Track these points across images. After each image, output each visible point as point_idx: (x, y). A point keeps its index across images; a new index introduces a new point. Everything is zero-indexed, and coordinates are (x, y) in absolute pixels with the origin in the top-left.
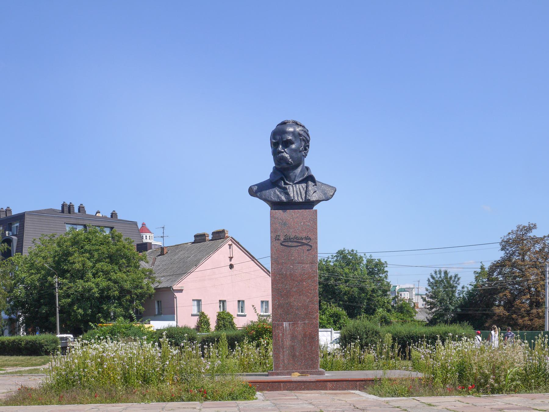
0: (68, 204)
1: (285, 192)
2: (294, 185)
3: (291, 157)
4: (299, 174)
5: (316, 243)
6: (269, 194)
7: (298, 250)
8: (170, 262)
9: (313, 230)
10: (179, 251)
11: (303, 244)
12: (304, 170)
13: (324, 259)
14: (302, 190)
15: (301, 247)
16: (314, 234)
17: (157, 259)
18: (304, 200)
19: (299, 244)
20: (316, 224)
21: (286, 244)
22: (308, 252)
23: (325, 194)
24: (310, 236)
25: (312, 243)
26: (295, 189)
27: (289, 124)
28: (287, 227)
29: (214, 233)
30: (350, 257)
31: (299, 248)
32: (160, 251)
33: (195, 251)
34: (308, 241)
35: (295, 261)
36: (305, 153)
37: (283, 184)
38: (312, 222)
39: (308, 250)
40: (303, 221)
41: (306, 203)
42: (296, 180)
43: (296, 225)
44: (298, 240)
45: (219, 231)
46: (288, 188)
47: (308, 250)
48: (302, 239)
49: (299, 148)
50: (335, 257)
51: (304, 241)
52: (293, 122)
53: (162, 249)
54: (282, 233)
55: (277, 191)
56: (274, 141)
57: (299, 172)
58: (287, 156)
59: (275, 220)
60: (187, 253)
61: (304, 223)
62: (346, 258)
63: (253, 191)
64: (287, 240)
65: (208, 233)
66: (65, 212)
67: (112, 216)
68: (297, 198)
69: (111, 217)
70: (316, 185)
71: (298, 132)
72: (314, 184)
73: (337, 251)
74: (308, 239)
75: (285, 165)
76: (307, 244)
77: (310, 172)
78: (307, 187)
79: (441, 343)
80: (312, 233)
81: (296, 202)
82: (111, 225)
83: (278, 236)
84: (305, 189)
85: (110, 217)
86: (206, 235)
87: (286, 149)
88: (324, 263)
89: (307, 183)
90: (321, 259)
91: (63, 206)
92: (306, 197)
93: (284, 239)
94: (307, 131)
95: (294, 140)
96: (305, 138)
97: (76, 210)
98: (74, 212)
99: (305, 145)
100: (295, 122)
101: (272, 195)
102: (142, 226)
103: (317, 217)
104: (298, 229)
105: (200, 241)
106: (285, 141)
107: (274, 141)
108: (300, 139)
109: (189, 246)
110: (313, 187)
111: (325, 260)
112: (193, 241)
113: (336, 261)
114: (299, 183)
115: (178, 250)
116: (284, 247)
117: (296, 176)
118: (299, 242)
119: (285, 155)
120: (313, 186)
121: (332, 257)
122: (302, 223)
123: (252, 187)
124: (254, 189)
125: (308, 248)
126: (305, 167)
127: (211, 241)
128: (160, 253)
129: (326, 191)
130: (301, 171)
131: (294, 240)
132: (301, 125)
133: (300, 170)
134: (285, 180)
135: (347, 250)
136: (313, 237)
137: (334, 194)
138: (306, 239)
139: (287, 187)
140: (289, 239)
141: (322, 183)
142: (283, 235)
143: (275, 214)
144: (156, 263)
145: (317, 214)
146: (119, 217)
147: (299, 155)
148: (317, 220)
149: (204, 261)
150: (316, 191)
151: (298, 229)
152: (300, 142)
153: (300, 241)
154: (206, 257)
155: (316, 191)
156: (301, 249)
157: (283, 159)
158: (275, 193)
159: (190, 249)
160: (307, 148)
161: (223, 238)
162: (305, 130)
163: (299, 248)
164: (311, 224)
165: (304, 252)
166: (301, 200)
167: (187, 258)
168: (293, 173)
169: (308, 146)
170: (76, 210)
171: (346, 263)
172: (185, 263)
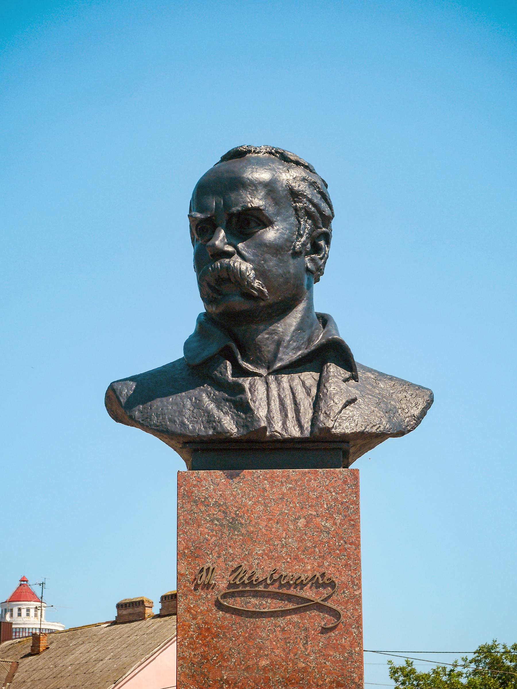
1: (234, 402)
2: (271, 378)
3: (260, 273)
4: (292, 336)
5: (358, 601)
6: (175, 408)
7: (283, 629)
8: (50, 673)
9: (346, 550)
10: (77, 645)
12: (311, 326)
13: (444, 669)
14: (301, 394)
15: (295, 618)
16: (346, 565)
17: (20, 666)
18: (307, 433)
19: (291, 606)
20: (355, 526)
21: (237, 603)
22: (323, 639)
23: (391, 412)
24: (331, 572)
25: (338, 602)
26: (274, 392)
27: (258, 158)
28: (242, 535)
29: (164, 599)
30: (509, 664)
31: (289, 623)
32: (30, 643)
33: (116, 643)
34: (326, 592)
35: (270, 675)
36: (312, 260)
37: (229, 372)
38: (338, 518)
39: (325, 630)
40: (304, 512)
41: (314, 442)
42: (281, 360)
43: (278, 530)
44: (284, 591)
46: (247, 386)
47: (325, 630)
48: (302, 585)
49: (289, 241)
50: (471, 663)
51: (308, 593)
52: (270, 153)
53: (36, 638)
54: (222, 559)
55: (207, 399)
56: (199, 215)
57: (293, 328)
58: (243, 268)
59: (195, 510)
60: (96, 649)
61: (309, 520)
62: (501, 664)
63: (120, 401)
64: (240, 589)
65: (151, 599)
68: (280, 424)
70: (355, 378)
71: (288, 185)
72: (348, 374)
73: (476, 648)
74: (324, 585)
76: (320, 607)
77: (334, 332)
78: (320, 384)
80: (341, 563)
81: (278, 441)
83: (204, 573)
84: (314, 391)
86: (146, 604)
87: (240, 245)
88: (444, 678)
89: (320, 371)
90: (438, 668)
92: (314, 420)
93: (230, 586)
94: (320, 183)
95: (270, 210)
96: (315, 205)
99: (315, 233)
100: (277, 152)
101: (188, 413)
102: (21, 585)
103: (358, 496)
104: (283, 546)
105: (131, 618)
106: (239, 214)
107: (199, 215)
108: (296, 209)
109: (102, 632)
110: (343, 385)
111: (448, 670)
112: (114, 619)
113: (475, 672)
115: (74, 643)
116: (228, 615)
117: (279, 344)
118: (290, 598)
119: (237, 262)
120: (346, 380)
121: (463, 663)
122: (302, 520)
123: (116, 386)
124: (121, 393)
125: (327, 620)
126: (315, 315)
127: (159, 619)
128: (28, 650)
129: (393, 400)
130: (300, 328)
131: (271, 589)
132: (298, 163)
133: (294, 324)
134: (239, 356)
135: (501, 647)
136: (343, 579)
137: (423, 413)
138: (318, 585)
139: (246, 382)
140: (251, 583)
141: (381, 374)
142: (227, 569)
143: (195, 486)
144: (16, 675)
145: (357, 486)
147: (292, 265)
148: (358, 509)
149: (136, 671)
150: (354, 400)
151: (283, 546)
152: (293, 219)
153: (292, 591)
154: (143, 660)
155: (354, 400)
156: (295, 625)
157: (229, 280)
158: (198, 405)
159: (104, 639)
160: (322, 243)
162: (312, 178)
163: (289, 623)
164: (335, 524)
165: (307, 637)
166: (296, 432)
167: (94, 663)
168: (270, 334)
169: (327, 237)
171: (499, 678)
172: (88, 676)
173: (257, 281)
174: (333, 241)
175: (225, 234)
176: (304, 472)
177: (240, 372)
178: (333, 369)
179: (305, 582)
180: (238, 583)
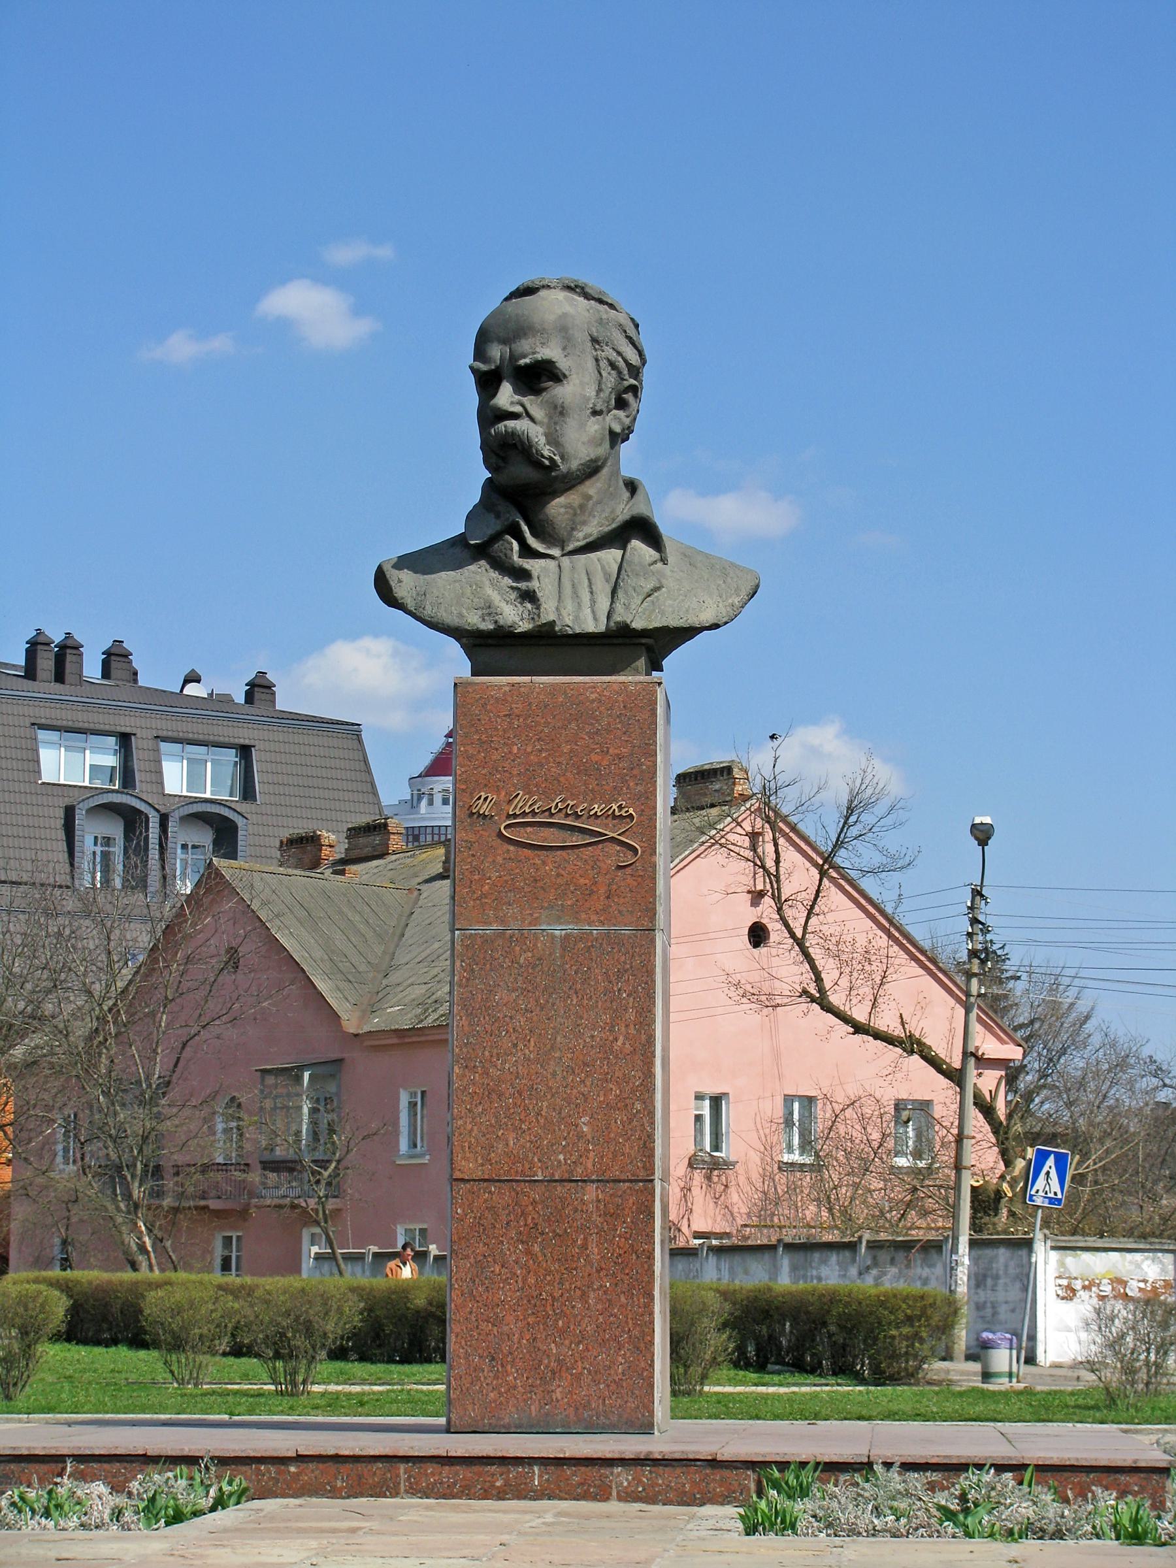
0: (58, 638)
11: (600, 839)
45: (706, 767)
66: (40, 674)
67: (249, 697)
69: (246, 702)
75: (521, 472)
79: (168, 1123)
82: (244, 736)
85: (240, 698)
89: (624, 548)
91: (35, 646)
97: (92, 669)
98: (81, 675)
99: (621, 388)
114: (592, 547)
146: (283, 703)
161: (725, 803)
169: (634, 390)
170: (92, 669)
173: (548, 447)
174: (645, 394)
175: (368, 642)
176: (614, 921)
177: (528, 552)
178: (636, 544)
179: (599, 814)
180: (518, 813)
